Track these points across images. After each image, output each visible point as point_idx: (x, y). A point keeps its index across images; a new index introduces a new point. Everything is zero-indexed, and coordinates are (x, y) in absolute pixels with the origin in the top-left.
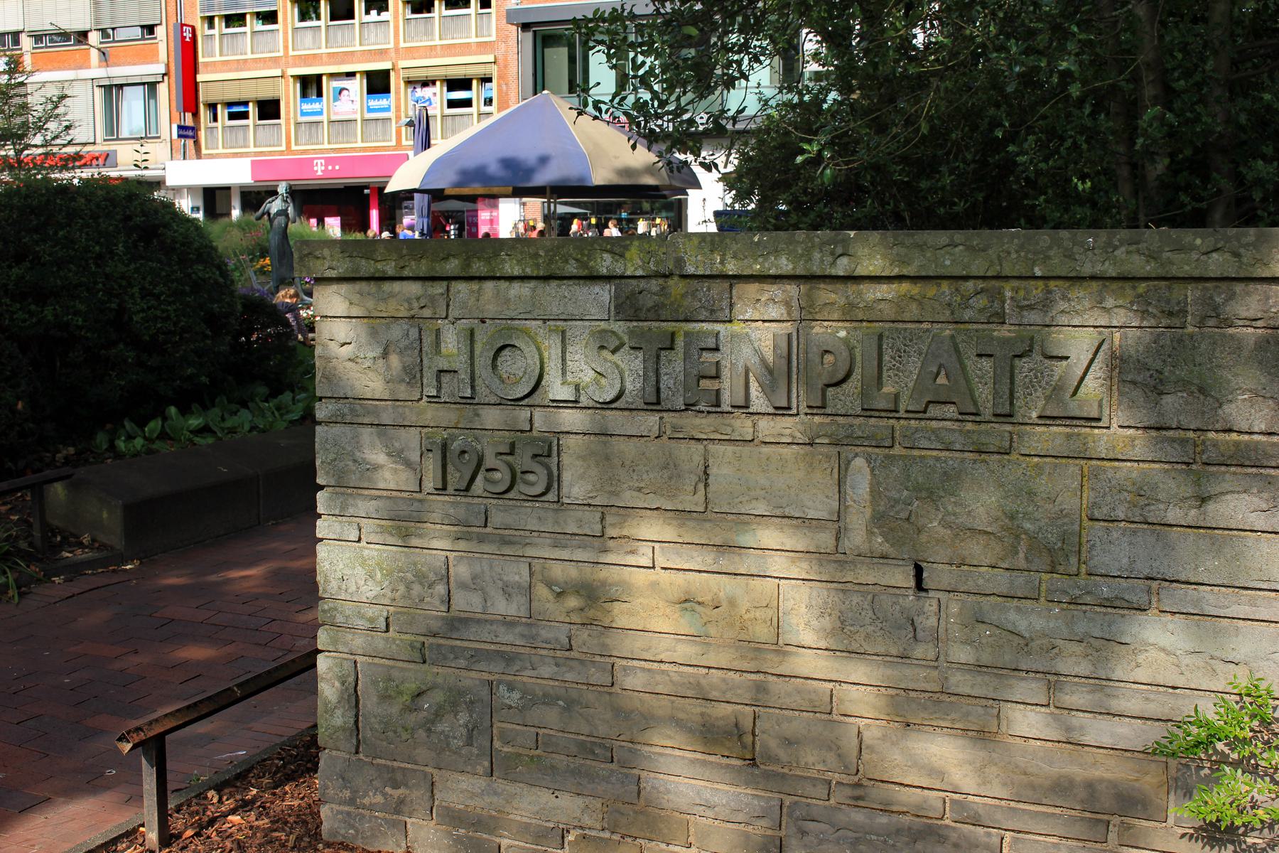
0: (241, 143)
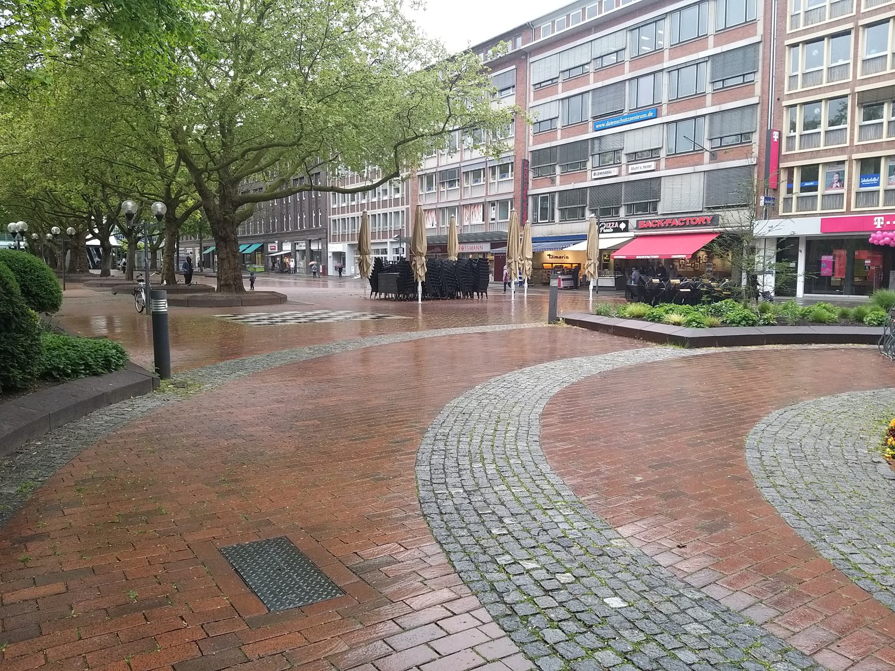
0: (810, 206)
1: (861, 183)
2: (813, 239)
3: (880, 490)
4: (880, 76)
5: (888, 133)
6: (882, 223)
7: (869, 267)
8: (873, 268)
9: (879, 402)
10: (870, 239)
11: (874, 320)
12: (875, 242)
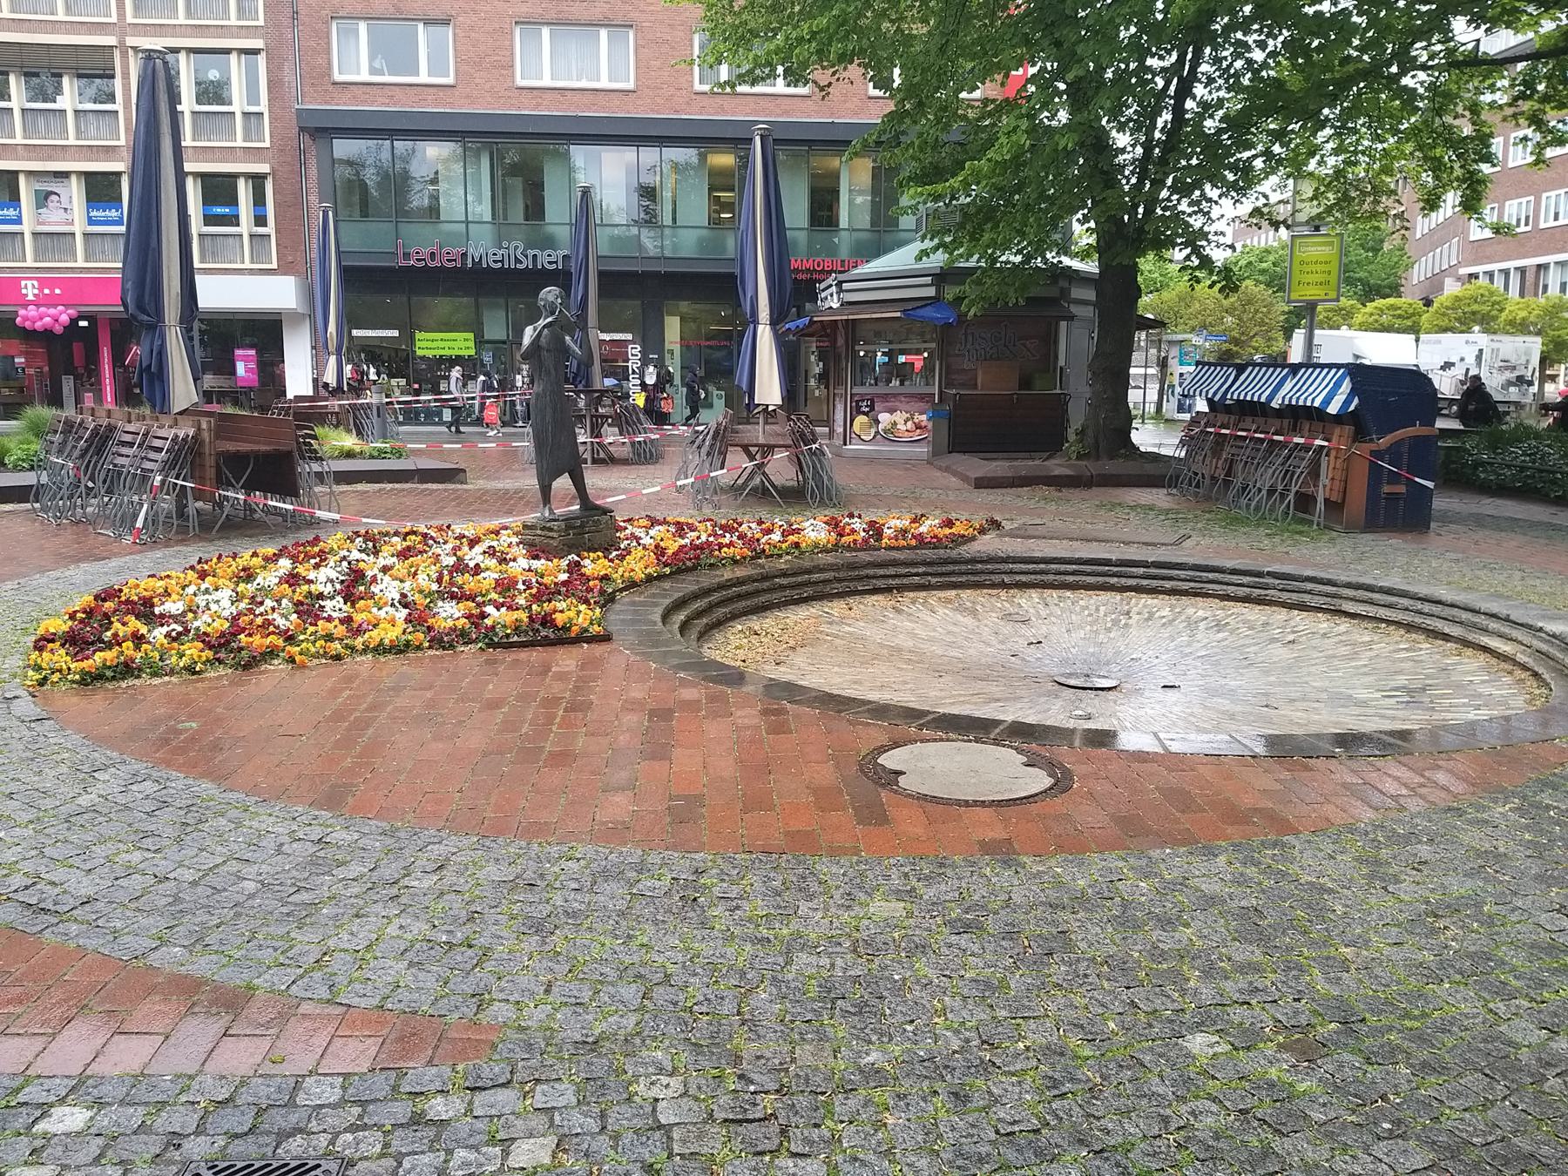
1: (89, 218)
2: (216, 317)
3: (14, 742)
4: (207, 26)
5: (25, 131)
6: (36, 291)
7: (23, 369)
8: (32, 371)
9: (26, 598)
10: (18, 320)
11: (23, 460)
12: (28, 324)
